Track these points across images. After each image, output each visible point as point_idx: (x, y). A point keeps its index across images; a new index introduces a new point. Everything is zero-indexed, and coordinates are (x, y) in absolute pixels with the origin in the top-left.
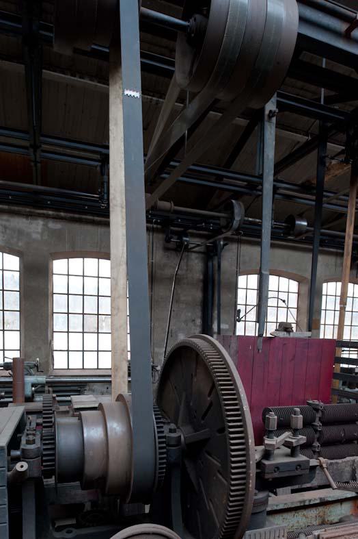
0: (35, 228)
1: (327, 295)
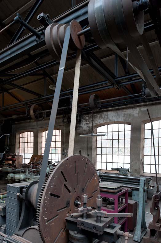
0: (135, 112)
1: (59, 135)
